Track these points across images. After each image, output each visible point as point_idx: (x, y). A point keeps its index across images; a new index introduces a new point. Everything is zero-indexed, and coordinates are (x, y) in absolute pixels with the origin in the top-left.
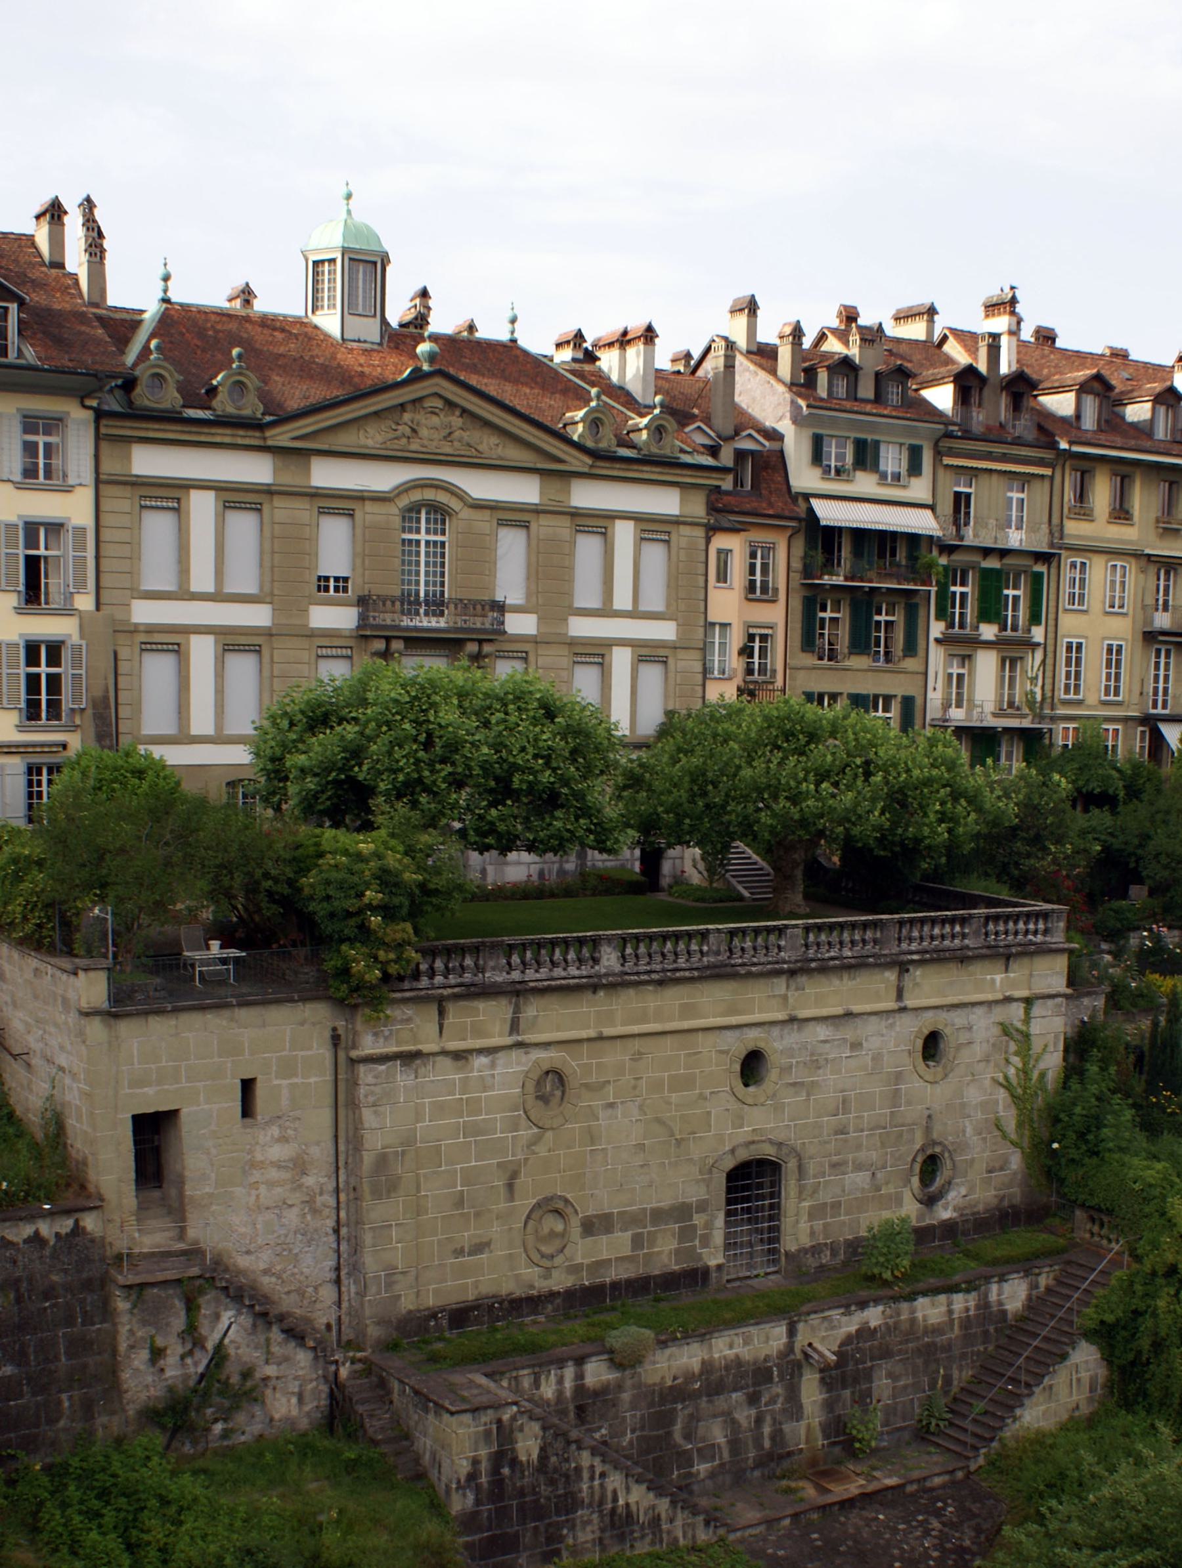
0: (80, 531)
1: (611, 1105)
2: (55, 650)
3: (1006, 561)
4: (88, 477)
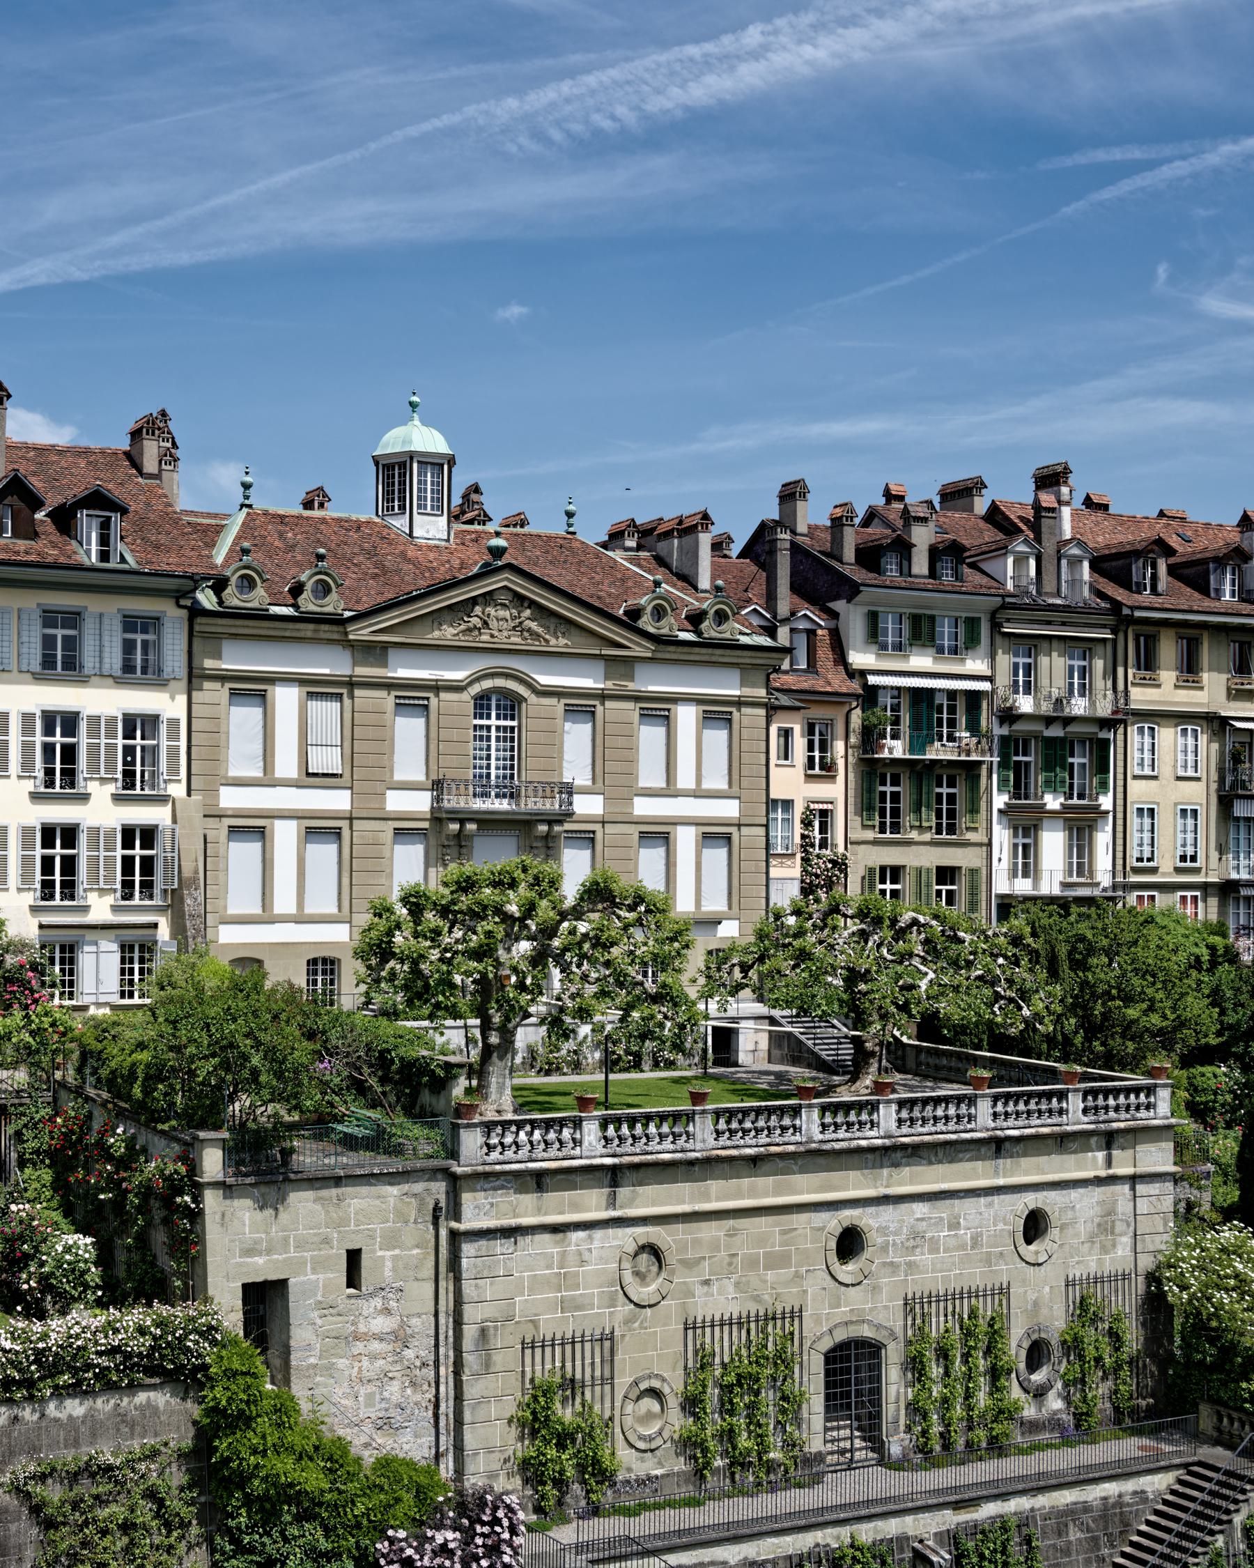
0: (174, 723)
1: (707, 1283)
2: (149, 835)
3: (1070, 729)
4: (182, 672)
